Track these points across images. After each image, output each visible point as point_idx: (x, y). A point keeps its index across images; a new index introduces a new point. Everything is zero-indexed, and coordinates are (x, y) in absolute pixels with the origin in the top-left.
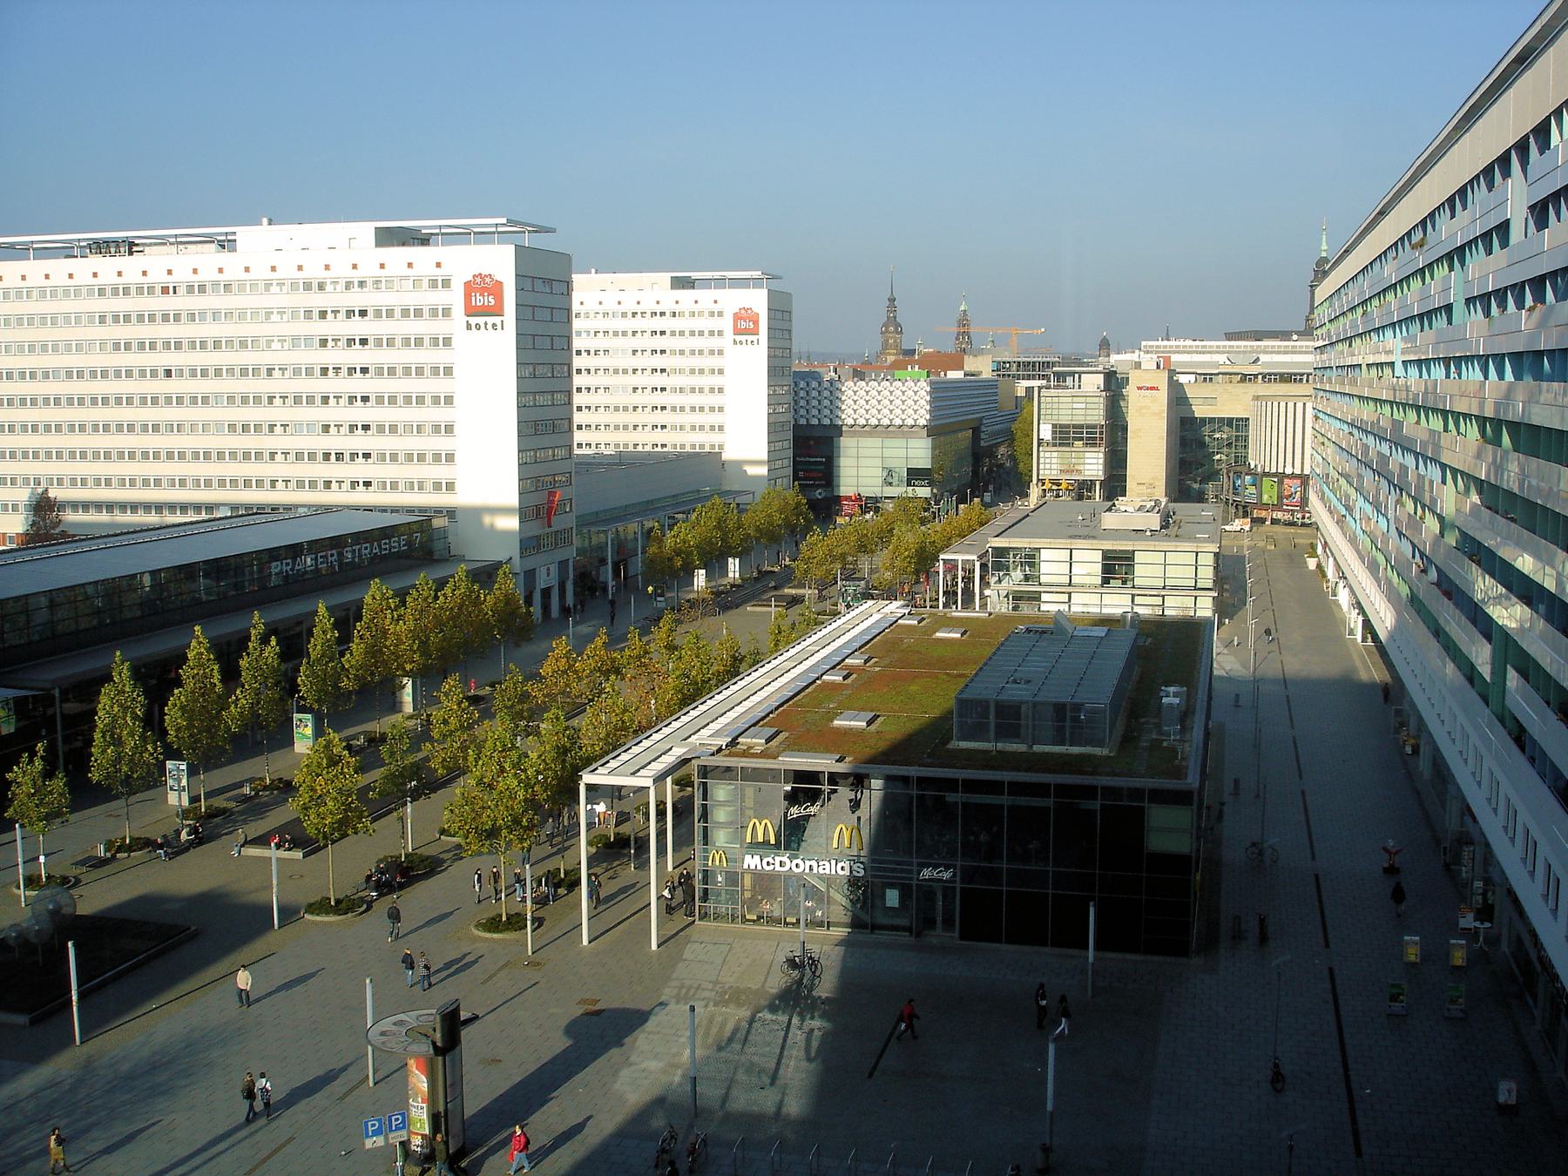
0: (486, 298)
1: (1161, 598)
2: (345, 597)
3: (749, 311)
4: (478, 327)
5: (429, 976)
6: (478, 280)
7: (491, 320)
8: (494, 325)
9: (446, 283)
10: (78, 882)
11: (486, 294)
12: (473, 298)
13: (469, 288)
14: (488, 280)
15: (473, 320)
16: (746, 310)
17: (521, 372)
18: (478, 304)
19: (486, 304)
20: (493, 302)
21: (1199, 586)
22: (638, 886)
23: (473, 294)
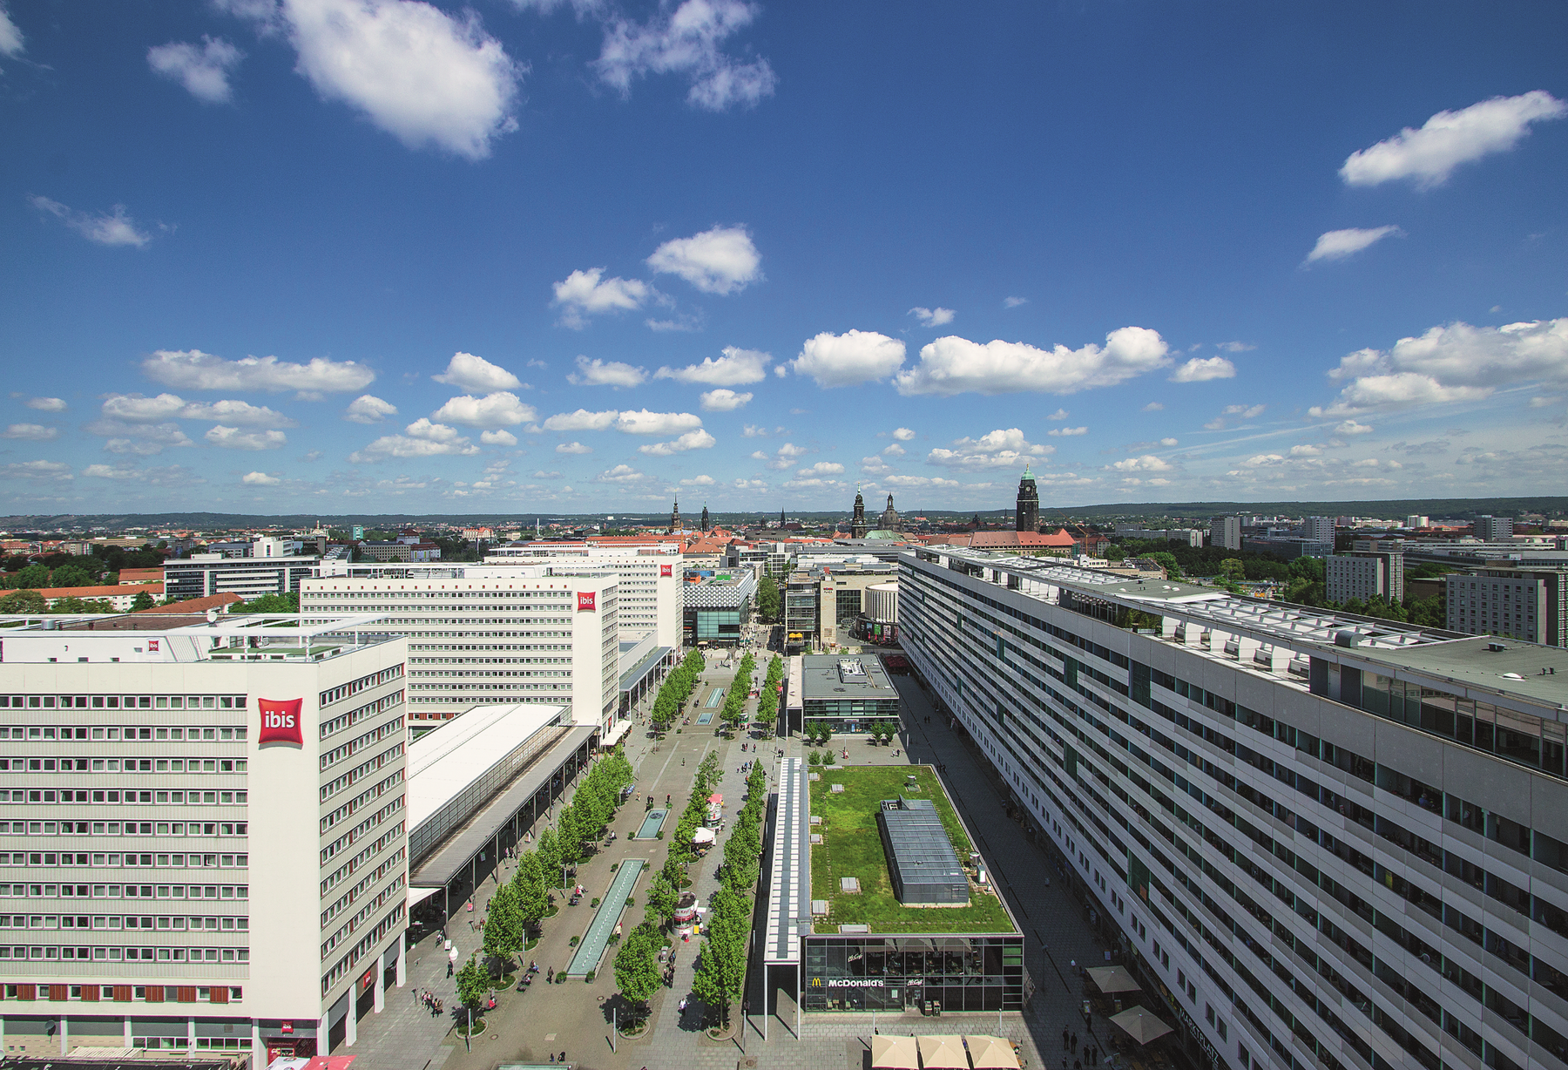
18: (273, 725)
19: (283, 726)
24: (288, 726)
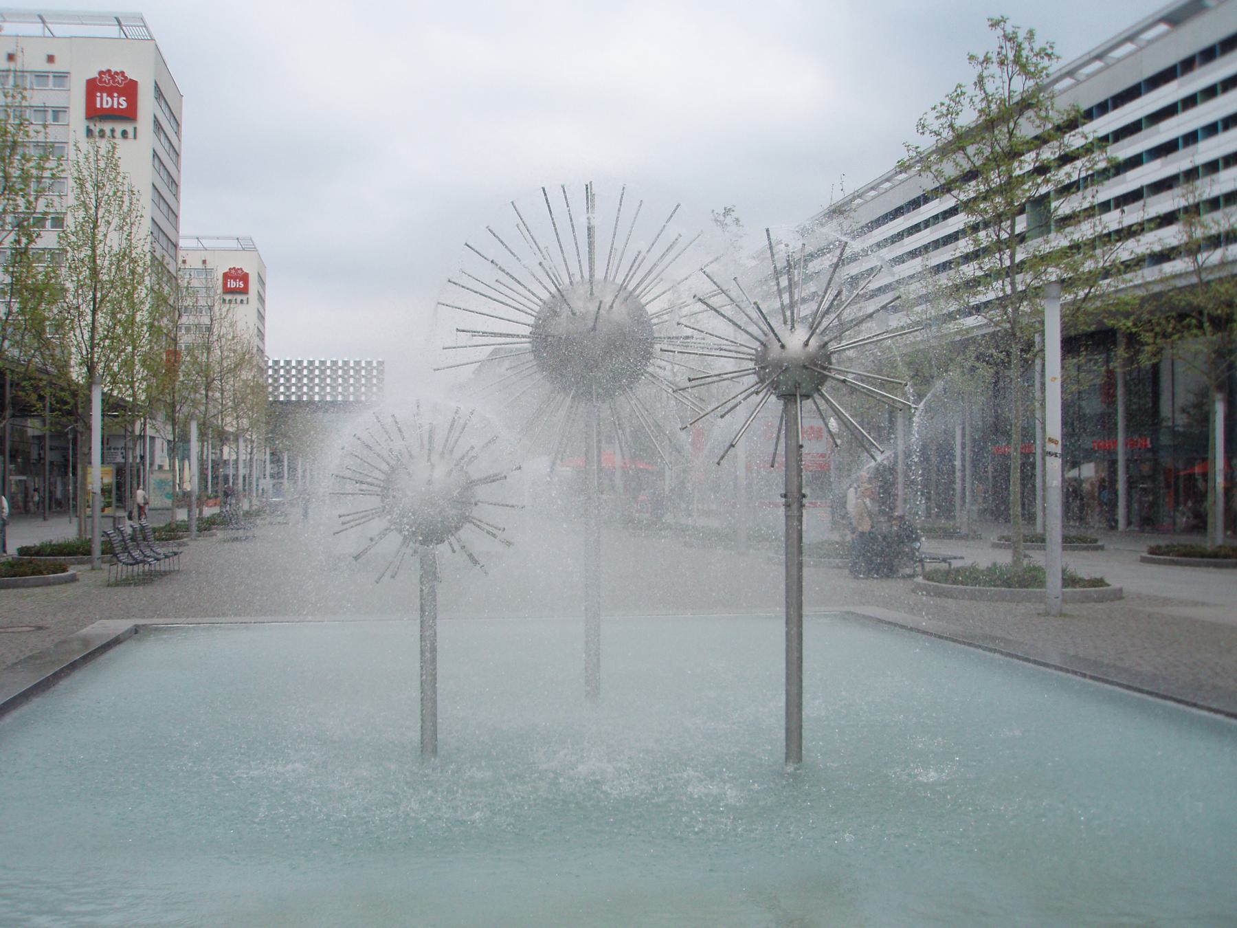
0: (115, 99)
1: (1048, 458)
2: (1047, 440)
3: (239, 272)
5: (792, 305)
6: (233, 272)
7: (239, 297)
8: (242, 301)
10: (992, 63)
11: (116, 95)
12: (98, 99)
13: (93, 87)
14: (119, 78)
15: (228, 297)
16: (236, 270)
17: (65, 490)
18: (105, 106)
20: (124, 105)
21: (1048, 458)
22: (643, 254)
23: (99, 94)
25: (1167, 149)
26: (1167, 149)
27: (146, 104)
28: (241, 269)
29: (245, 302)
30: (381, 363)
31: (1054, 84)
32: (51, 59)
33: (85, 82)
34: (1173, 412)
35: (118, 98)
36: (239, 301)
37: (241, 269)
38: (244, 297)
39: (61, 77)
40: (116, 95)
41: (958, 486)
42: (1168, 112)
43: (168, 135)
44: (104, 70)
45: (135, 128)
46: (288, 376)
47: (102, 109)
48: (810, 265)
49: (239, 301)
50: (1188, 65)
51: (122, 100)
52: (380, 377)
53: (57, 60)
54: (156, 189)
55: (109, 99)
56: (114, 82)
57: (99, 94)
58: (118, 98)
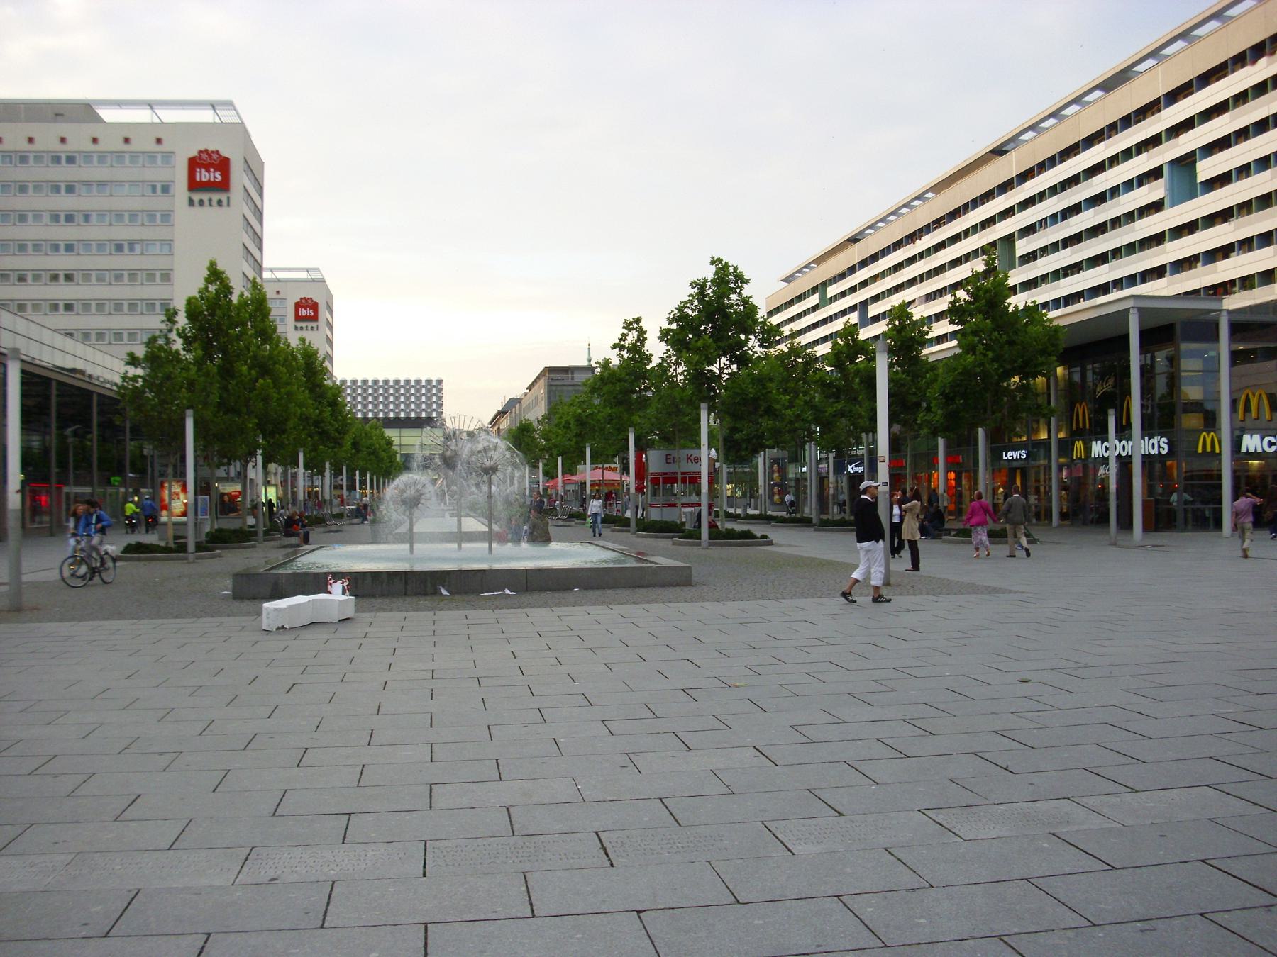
0: (212, 174)
4: (201, 203)
6: (204, 156)
8: (312, 328)
9: (168, 156)
12: (198, 174)
13: (194, 164)
14: (310, 301)
15: (299, 324)
18: (303, 315)
23: (198, 170)
24: (216, 180)
25: (1099, 199)
26: (1099, 199)
27: (238, 177)
28: (311, 299)
29: (315, 328)
30: (440, 382)
31: (1227, 10)
32: (278, 292)
33: (293, 305)
34: (331, 496)
35: (214, 172)
36: (309, 328)
37: (217, 152)
38: (314, 324)
39: (168, 156)
40: (212, 170)
41: (808, 491)
42: (1098, 169)
43: (254, 199)
44: (203, 149)
45: (228, 198)
46: (354, 395)
47: (201, 181)
48: (829, 289)
49: (309, 328)
50: (1113, 128)
51: (311, 312)
52: (439, 387)
53: (164, 142)
54: (246, 247)
55: (207, 174)
56: (211, 159)
57: (198, 170)
58: (214, 172)
